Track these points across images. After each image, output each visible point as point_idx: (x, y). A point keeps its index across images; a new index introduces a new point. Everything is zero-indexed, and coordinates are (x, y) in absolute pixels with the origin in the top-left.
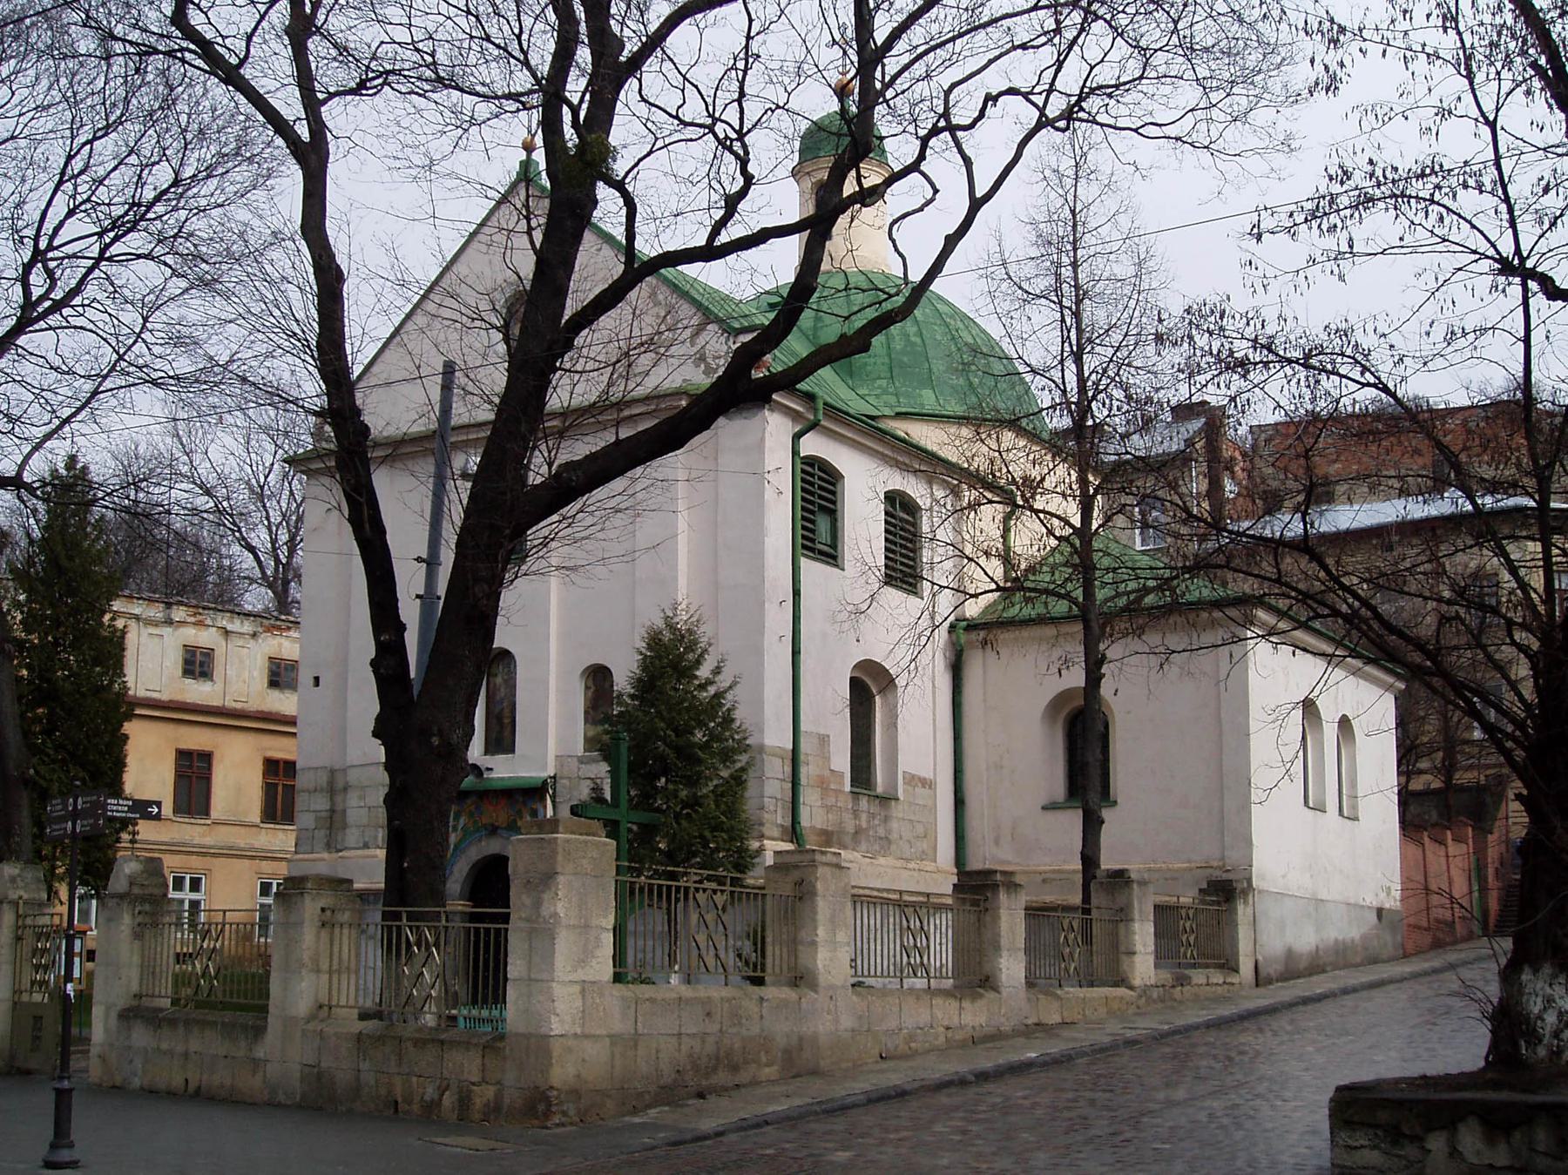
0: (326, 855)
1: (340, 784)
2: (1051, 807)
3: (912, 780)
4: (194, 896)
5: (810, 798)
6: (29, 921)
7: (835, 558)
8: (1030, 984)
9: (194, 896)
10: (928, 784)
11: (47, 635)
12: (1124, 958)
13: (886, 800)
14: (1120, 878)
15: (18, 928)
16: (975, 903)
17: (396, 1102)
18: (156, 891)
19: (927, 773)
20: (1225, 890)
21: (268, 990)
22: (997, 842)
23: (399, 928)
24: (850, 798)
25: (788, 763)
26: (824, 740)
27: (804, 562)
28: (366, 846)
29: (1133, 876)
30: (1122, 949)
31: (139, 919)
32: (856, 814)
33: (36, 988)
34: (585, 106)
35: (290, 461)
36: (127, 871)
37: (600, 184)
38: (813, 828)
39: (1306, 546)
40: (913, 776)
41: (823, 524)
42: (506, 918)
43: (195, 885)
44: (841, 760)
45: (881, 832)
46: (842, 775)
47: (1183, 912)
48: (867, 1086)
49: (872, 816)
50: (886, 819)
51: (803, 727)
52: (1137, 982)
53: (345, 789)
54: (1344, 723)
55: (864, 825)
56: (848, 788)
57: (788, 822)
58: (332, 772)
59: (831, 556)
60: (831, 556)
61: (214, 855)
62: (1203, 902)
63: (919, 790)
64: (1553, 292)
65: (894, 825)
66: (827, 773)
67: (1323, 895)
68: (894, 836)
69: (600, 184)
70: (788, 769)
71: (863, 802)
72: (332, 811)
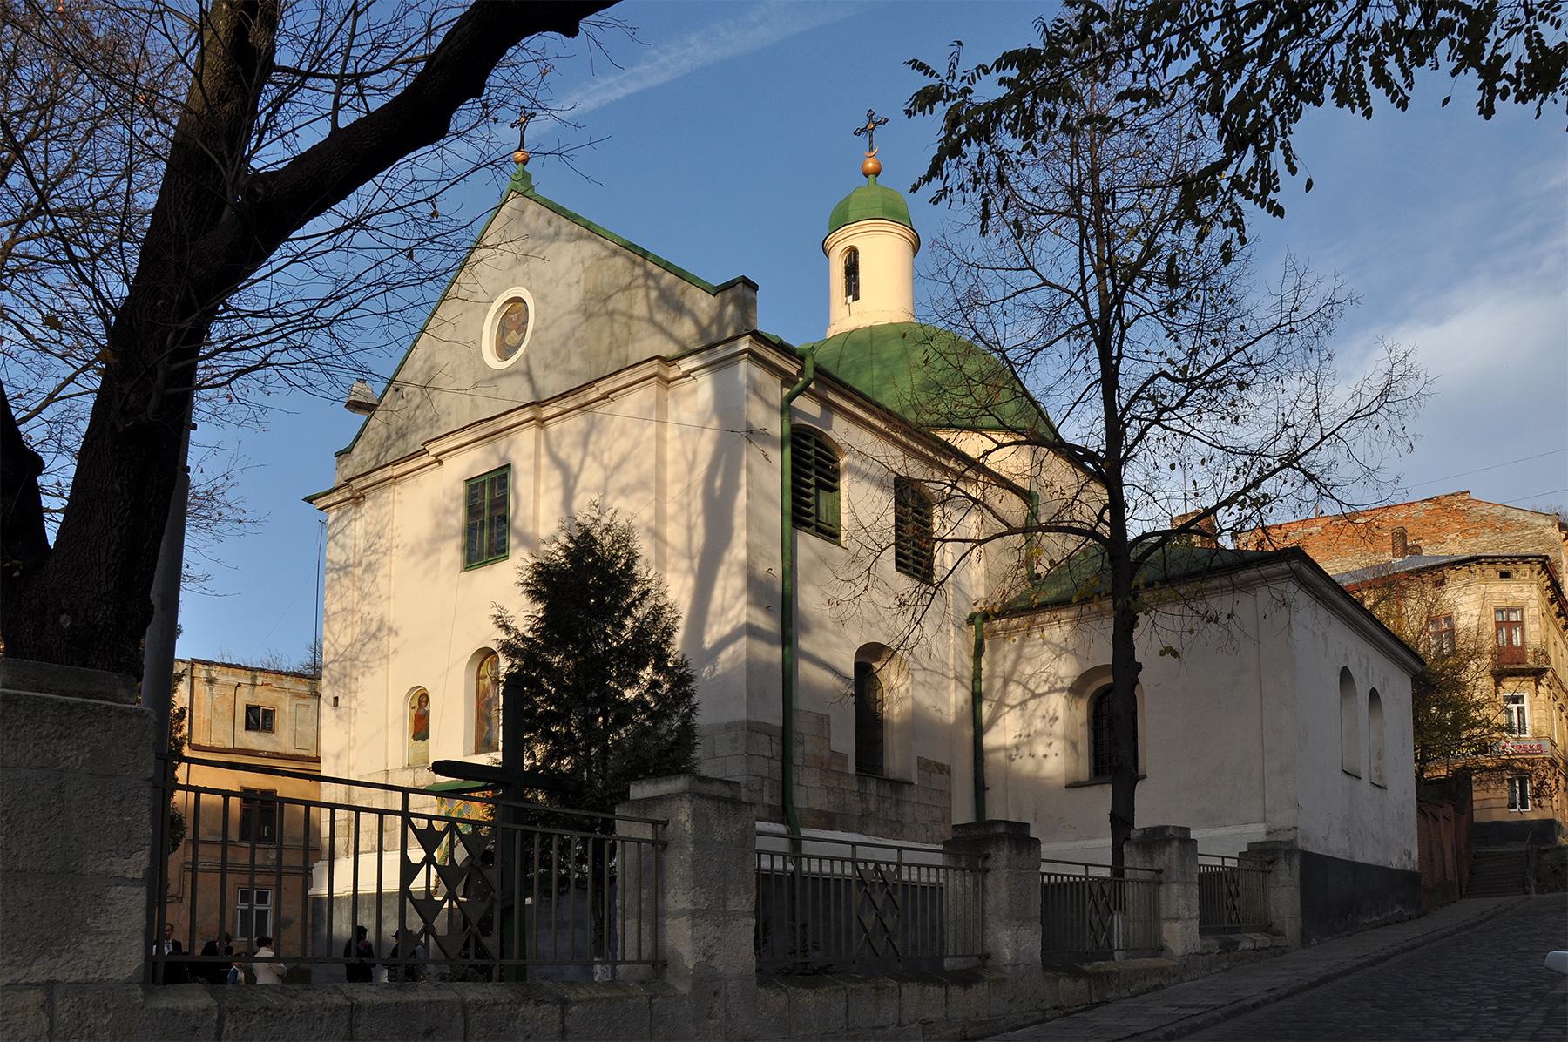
3: (926, 765)
8: (1046, 964)
10: (945, 770)
13: (899, 785)
21: (263, 792)
24: (854, 781)
25: (777, 740)
26: (823, 721)
30: (1163, 915)
32: (862, 796)
34: (995, 437)
35: (1545, 670)
37: (1134, 530)
38: (810, 810)
39: (1360, 82)
40: (929, 762)
45: (892, 815)
46: (844, 757)
47: (1095, 888)
50: (898, 803)
54: (1374, 695)
55: (873, 808)
56: (852, 769)
57: (778, 802)
63: (936, 776)
64: (243, 62)
66: (826, 754)
68: (908, 819)
69: (1134, 530)
70: (777, 748)
71: (872, 787)
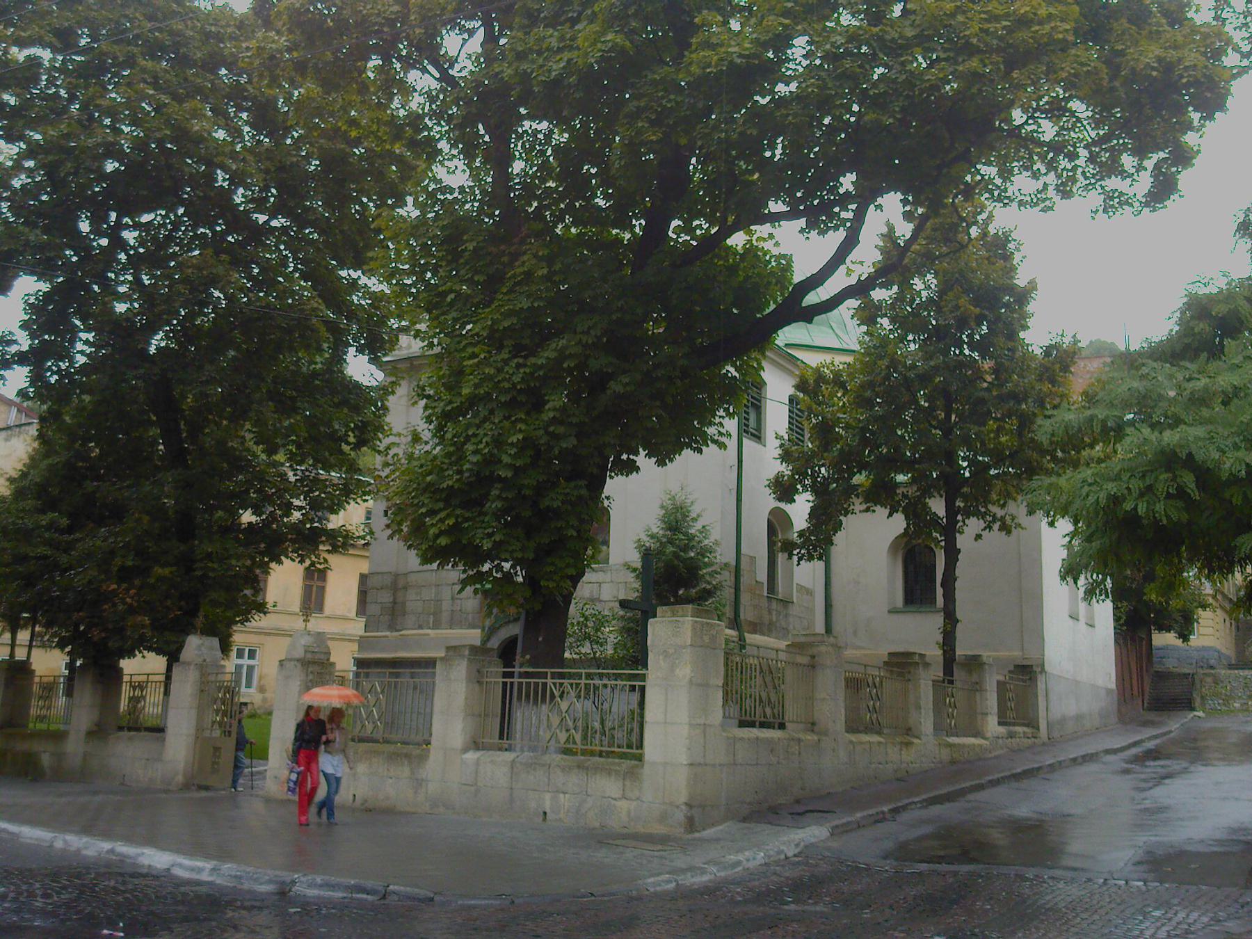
0: (388, 633)
1: (401, 583)
2: (893, 611)
4: (251, 662)
5: (745, 598)
6: (212, 678)
7: (759, 438)
9: (251, 662)
10: (809, 592)
11: (836, 481)
12: (979, 717)
14: (974, 663)
15: (202, 683)
16: (901, 674)
17: (545, 813)
18: (322, 657)
19: (808, 585)
20: (1027, 673)
22: (855, 633)
23: (545, 685)
26: (753, 559)
27: (745, 441)
28: (420, 627)
29: (985, 659)
31: (311, 677)
33: (216, 726)
36: (303, 642)
41: (752, 417)
42: (643, 678)
43: (252, 655)
44: (762, 576)
48: (957, 804)
49: (779, 613)
50: (786, 616)
51: (744, 550)
52: (989, 735)
53: (405, 588)
58: (397, 575)
59: (758, 437)
60: (758, 437)
61: (266, 634)
62: (1011, 678)
65: (791, 620)
67: (1078, 679)
72: (395, 603)
